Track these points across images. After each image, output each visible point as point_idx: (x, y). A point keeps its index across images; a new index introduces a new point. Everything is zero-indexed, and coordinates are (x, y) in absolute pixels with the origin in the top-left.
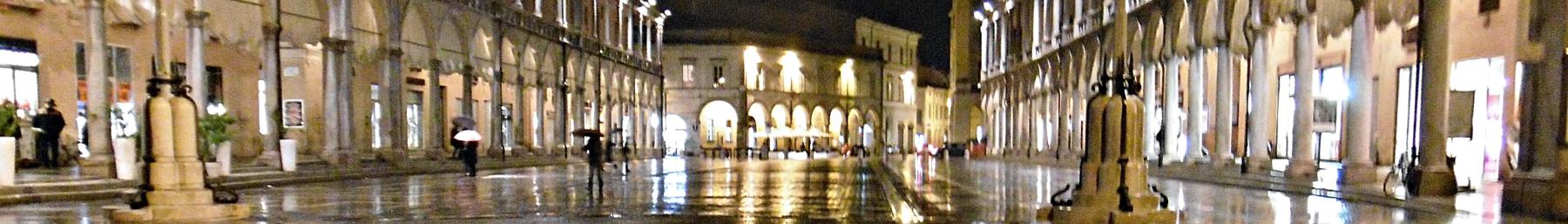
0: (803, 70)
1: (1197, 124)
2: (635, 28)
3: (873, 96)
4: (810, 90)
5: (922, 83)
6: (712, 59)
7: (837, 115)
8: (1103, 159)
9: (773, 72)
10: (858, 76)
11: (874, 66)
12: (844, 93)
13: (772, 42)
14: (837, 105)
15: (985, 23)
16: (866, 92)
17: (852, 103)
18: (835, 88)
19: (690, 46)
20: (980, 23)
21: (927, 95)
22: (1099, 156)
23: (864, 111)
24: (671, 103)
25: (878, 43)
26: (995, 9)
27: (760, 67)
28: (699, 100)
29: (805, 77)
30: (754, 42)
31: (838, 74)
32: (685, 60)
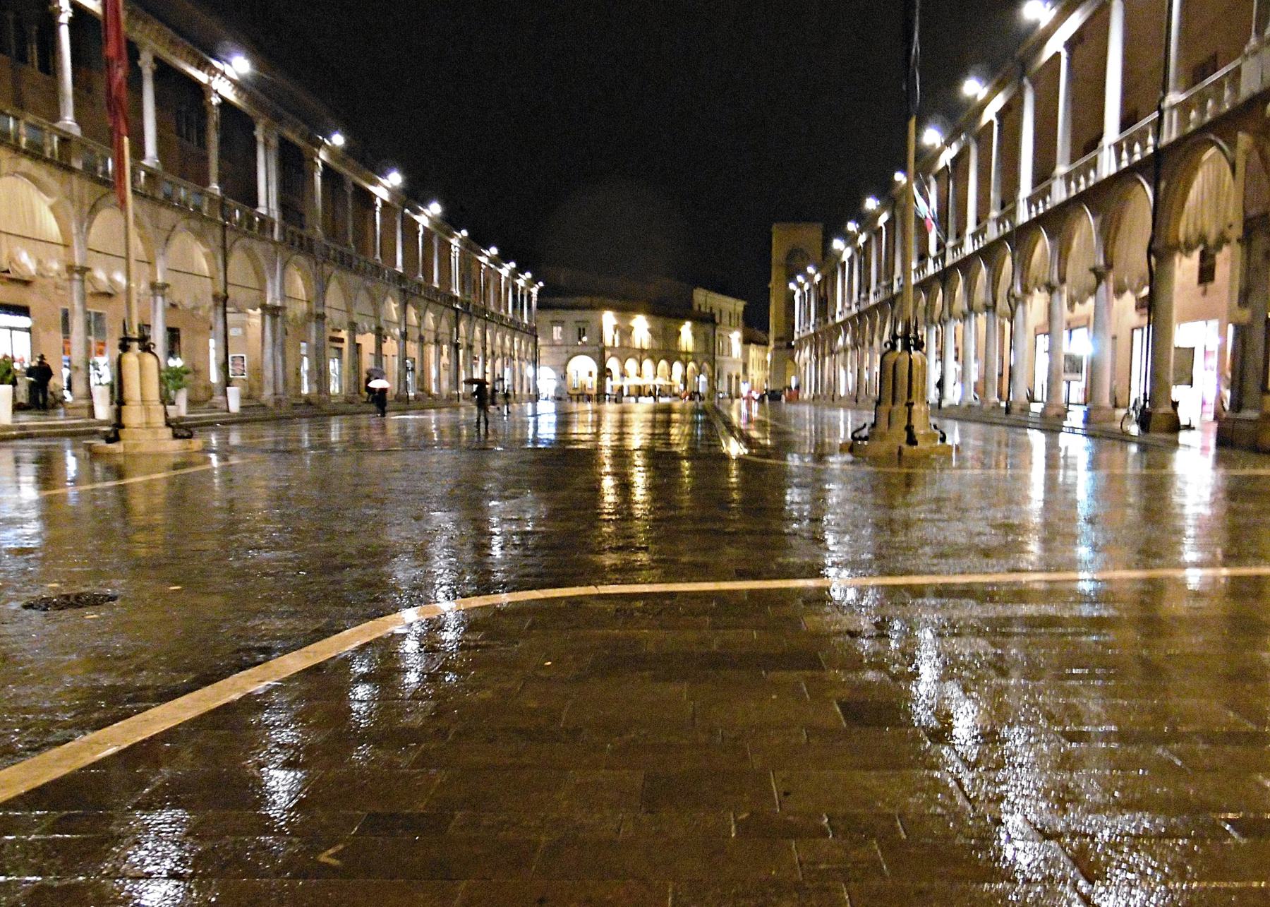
0: (650, 331)
2: (515, 297)
4: (656, 347)
5: (747, 341)
7: (678, 367)
8: (893, 403)
9: (626, 332)
10: (695, 335)
11: (708, 327)
12: (683, 349)
13: (625, 308)
14: (678, 359)
15: (798, 293)
16: (701, 348)
17: (690, 357)
18: (676, 345)
20: (794, 293)
21: (751, 351)
22: (890, 400)
27: (616, 328)
30: (610, 307)
31: (679, 334)
32: (555, 322)
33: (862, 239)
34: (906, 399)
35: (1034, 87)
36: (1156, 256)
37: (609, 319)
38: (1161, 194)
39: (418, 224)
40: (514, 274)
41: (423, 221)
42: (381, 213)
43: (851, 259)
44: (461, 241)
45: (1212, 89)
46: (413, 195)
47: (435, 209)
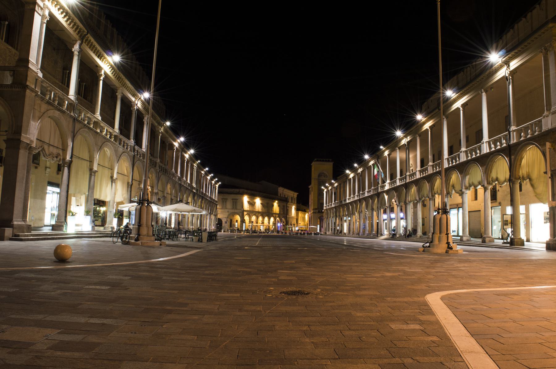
0: (261, 204)
2: (211, 188)
3: (284, 213)
4: (264, 211)
5: (298, 210)
6: (232, 199)
7: (272, 219)
9: (252, 204)
11: (285, 204)
13: (252, 196)
14: (273, 216)
15: (325, 190)
16: (282, 213)
18: (272, 210)
20: (323, 190)
21: (299, 213)
23: (281, 218)
25: (285, 195)
28: (228, 213)
29: (263, 206)
30: (247, 194)
33: (360, 170)
35: (447, 119)
36: (512, 183)
38: (512, 160)
40: (212, 179)
41: (187, 156)
42: (176, 152)
43: (354, 178)
44: (197, 165)
45: (530, 126)
46: (185, 146)
47: (192, 151)
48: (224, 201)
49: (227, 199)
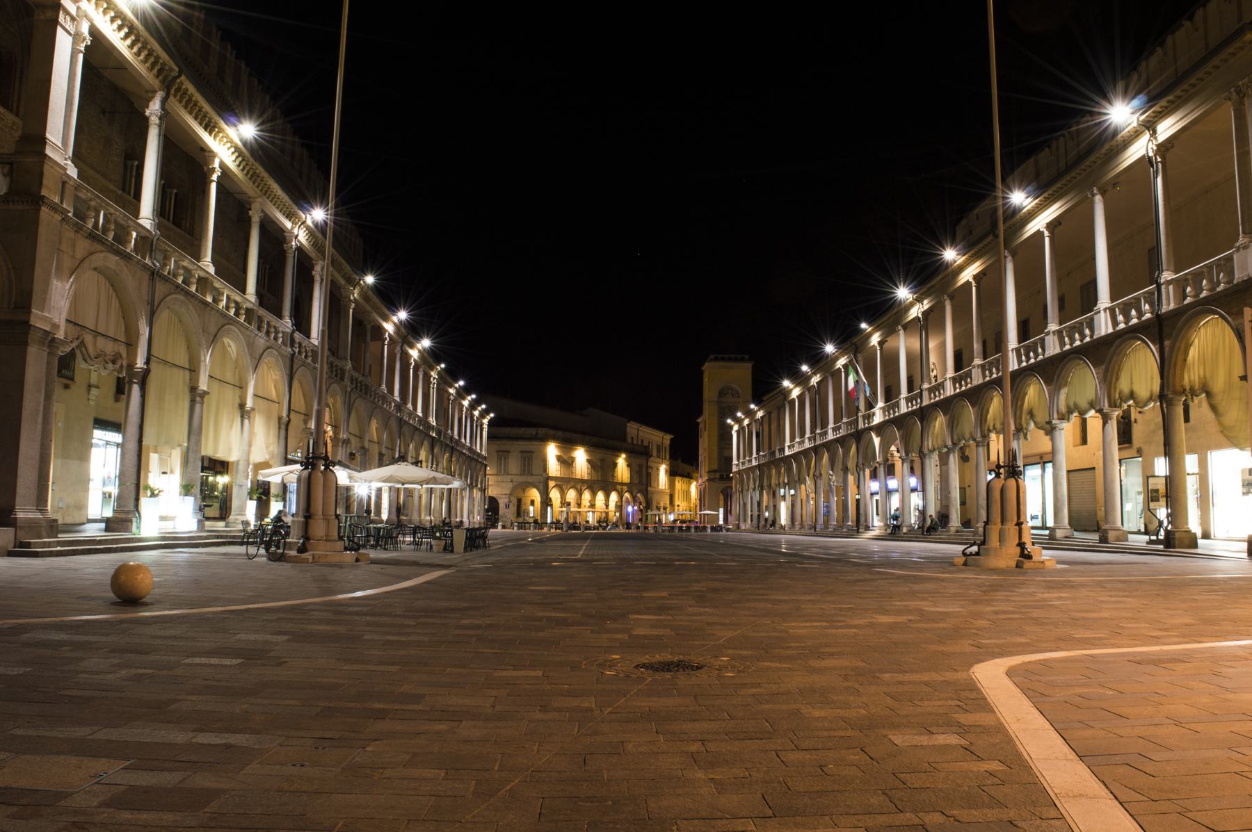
0: (588, 461)
1: (434, 571)
4: (595, 478)
5: (672, 473)
6: (521, 452)
7: (614, 497)
8: (1003, 522)
9: (566, 462)
13: (567, 443)
15: (736, 427)
18: (613, 476)
19: (504, 442)
20: (731, 427)
21: (677, 482)
22: (999, 520)
23: (634, 495)
24: (492, 485)
26: (746, 417)
34: (1016, 519)
35: (1013, 257)
37: (552, 451)
38: (1167, 350)
39: (411, 356)
40: (473, 405)
41: (414, 354)
42: (388, 346)
43: (801, 397)
46: (411, 331)
47: (426, 343)
48: (502, 456)
49: (509, 452)
